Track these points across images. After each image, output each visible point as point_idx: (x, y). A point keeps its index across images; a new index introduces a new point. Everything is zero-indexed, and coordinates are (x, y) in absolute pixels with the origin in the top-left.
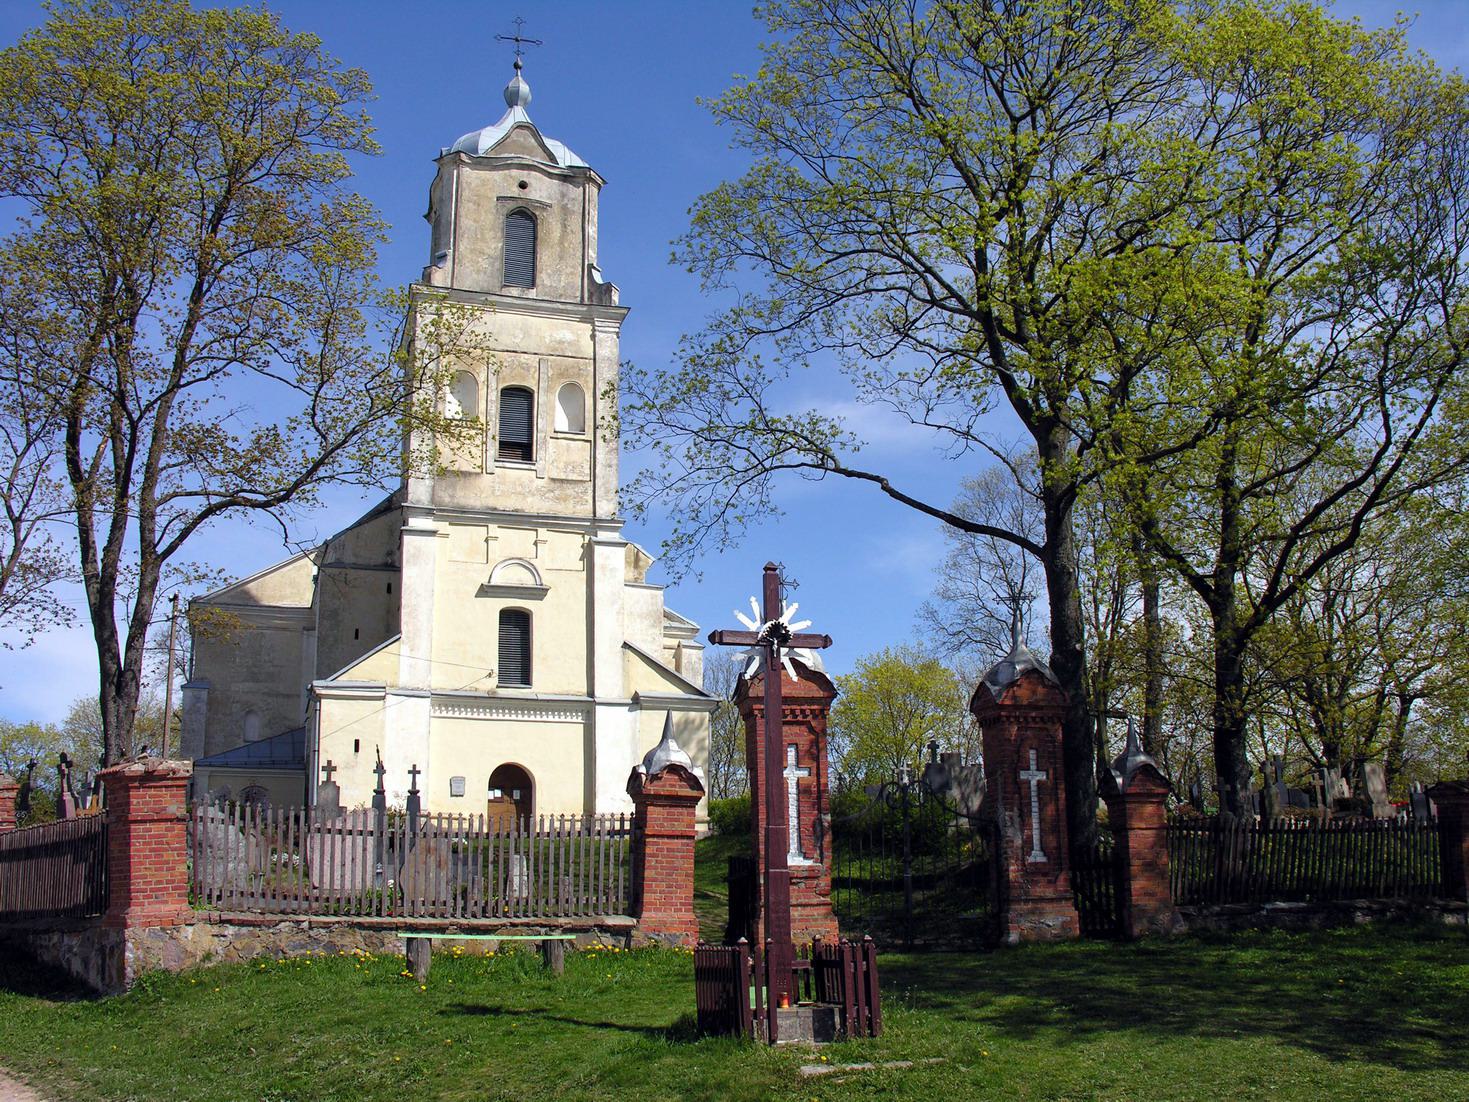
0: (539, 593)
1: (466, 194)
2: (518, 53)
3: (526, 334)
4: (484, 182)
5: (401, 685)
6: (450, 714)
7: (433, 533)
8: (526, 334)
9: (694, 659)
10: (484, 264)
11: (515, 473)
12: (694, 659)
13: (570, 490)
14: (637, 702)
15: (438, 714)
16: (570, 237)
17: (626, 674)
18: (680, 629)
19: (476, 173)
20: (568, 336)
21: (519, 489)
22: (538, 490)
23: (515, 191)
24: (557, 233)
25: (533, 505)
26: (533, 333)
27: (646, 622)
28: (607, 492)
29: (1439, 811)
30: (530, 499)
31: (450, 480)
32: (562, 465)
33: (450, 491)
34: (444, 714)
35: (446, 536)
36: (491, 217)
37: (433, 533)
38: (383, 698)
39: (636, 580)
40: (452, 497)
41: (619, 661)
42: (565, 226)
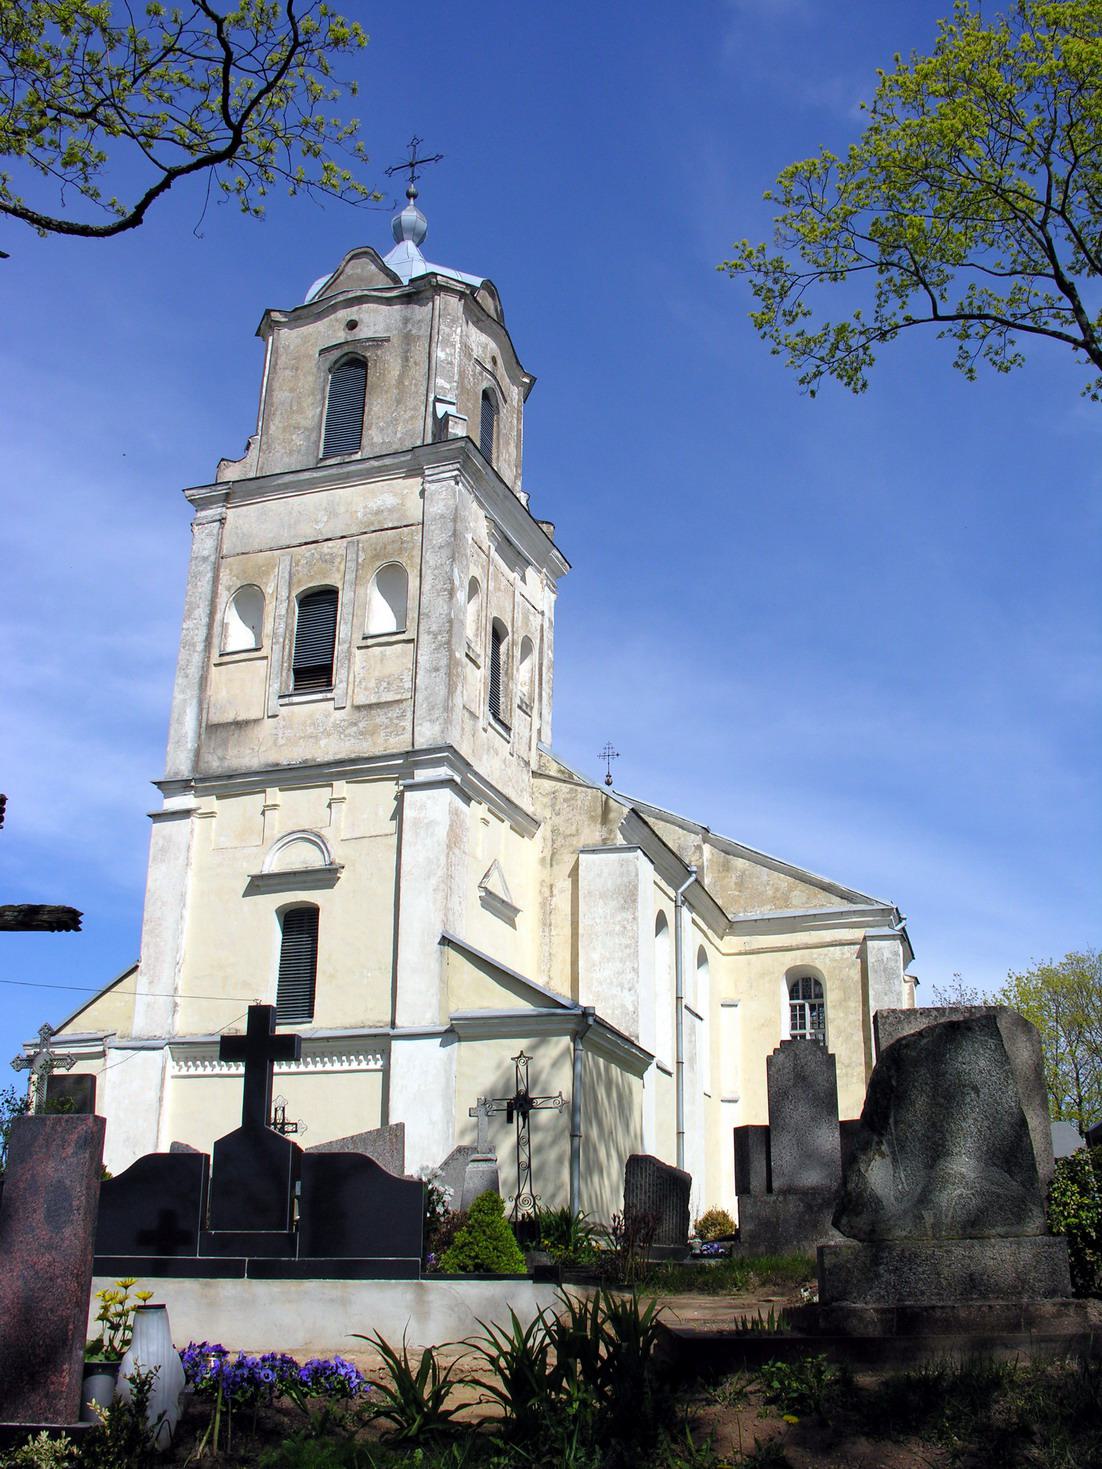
0: (327, 877)
1: (283, 360)
2: (412, 179)
3: (332, 513)
4: (305, 339)
5: (135, 1033)
6: (200, 1071)
7: (186, 813)
8: (332, 513)
9: (887, 954)
10: (298, 440)
11: (312, 709)
12: (887, 954)
13: (380, 717)
14: (456, 1032)
15: (184, 1072)
16: (412, 372)
17: (444, 984)
18: (862, 913)
19: (295, 332)
20: (389, 500)
21: (310, 730)
22: (335, 726)
23: (342, 335)
24: (394, 372)
25: (328, 749)
26: (342, 509)
27: (613, 904)
28: (432, 708)
29: (511, 1374)
30: (323, 743)
31: (222, 734)
32: (372, 684)
33: (220, 753)
34: (192, 1071)
35: (211, 815)
36: (311, 379)
37: (186, 813)
38: (103, 1054)
39: (604, 841)
40: (222, 759)
41: (434, 966)
42: (406, 359)
